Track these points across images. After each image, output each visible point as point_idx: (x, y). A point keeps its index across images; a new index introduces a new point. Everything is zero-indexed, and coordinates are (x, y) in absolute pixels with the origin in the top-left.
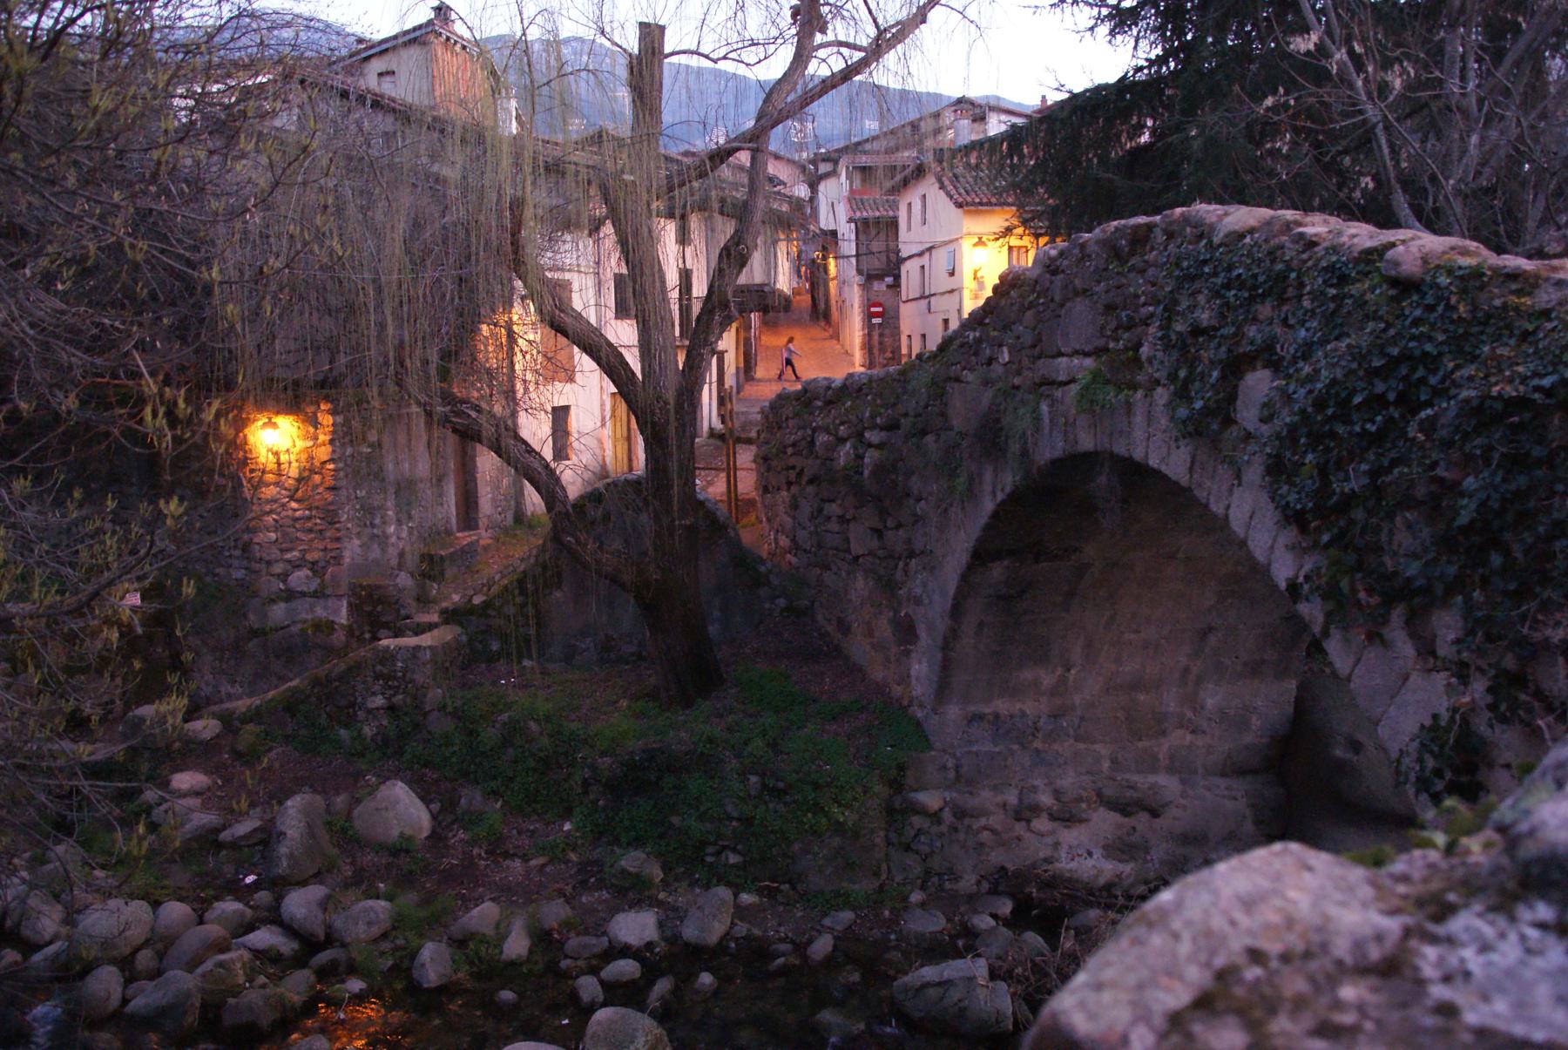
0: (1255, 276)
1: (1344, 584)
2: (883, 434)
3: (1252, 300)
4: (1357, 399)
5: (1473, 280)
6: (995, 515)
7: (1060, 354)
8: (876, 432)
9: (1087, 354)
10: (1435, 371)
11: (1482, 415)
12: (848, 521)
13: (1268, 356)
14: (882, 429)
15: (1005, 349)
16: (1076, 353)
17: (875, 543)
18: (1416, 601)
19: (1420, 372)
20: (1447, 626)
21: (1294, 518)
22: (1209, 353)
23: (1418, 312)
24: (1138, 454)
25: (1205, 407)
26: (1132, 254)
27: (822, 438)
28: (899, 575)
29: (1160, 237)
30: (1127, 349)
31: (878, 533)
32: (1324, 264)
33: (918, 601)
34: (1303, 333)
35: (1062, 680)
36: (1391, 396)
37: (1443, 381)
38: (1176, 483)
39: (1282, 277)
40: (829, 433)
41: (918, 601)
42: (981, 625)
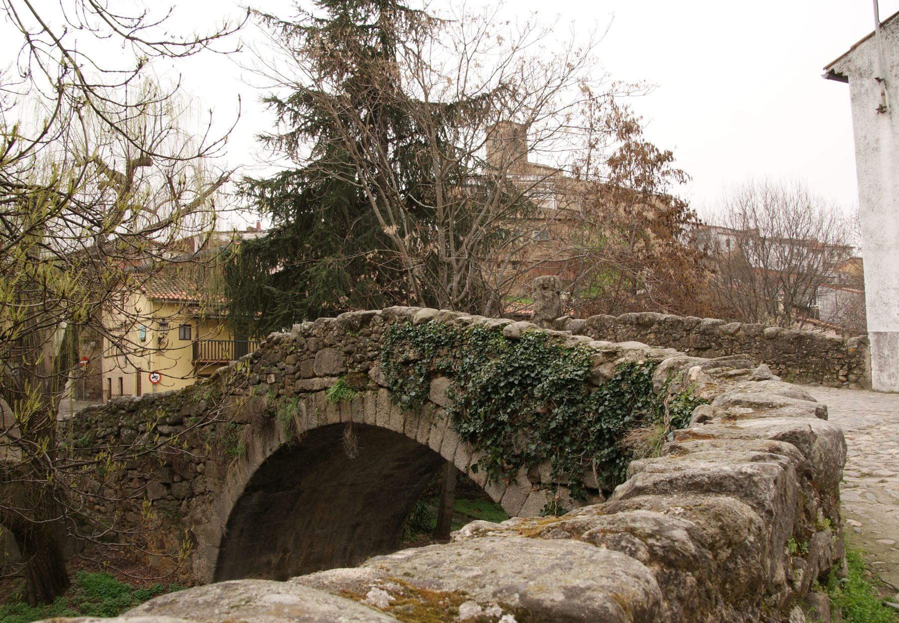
0: (439, 337)
1: (498, 461)
2: (170, 428)
3: (436, 348)
4: (502, 384)
5: (542, 338)
6: (263, 465)
7: (314, 376)
8: (165, 427)
9: (333, 376)
10: (533, 372)
11: (558, 386)
12: (146, 480)
13: (448, 373)
14: (170, 425)
15: (272, 376)
16: (326, 375)
17: (165, 492)
18: (533, 462)
19: (527, 373)
20: (546, 474)
21: (470, 438)
22: (412, 372)
23: (522, 350)
24: (370, 421)
25: (417, 395)
26: (361, 327)
27: (126, 432)
28: (183, 508)
29: (379, 319)
30: (360, 372)
31: (168, 486)
32: (475, 331)
33: (198, 522)
34: (468, 360)
35: (283, 559)
36: (516, 382)
37: (537, 375)
38: (396, 432)
39: (452, 338)
40: (132, 428)
41: (198, 522)
42: (242, 531)
